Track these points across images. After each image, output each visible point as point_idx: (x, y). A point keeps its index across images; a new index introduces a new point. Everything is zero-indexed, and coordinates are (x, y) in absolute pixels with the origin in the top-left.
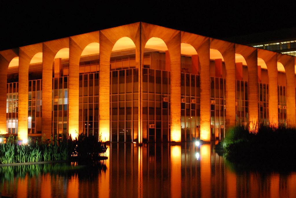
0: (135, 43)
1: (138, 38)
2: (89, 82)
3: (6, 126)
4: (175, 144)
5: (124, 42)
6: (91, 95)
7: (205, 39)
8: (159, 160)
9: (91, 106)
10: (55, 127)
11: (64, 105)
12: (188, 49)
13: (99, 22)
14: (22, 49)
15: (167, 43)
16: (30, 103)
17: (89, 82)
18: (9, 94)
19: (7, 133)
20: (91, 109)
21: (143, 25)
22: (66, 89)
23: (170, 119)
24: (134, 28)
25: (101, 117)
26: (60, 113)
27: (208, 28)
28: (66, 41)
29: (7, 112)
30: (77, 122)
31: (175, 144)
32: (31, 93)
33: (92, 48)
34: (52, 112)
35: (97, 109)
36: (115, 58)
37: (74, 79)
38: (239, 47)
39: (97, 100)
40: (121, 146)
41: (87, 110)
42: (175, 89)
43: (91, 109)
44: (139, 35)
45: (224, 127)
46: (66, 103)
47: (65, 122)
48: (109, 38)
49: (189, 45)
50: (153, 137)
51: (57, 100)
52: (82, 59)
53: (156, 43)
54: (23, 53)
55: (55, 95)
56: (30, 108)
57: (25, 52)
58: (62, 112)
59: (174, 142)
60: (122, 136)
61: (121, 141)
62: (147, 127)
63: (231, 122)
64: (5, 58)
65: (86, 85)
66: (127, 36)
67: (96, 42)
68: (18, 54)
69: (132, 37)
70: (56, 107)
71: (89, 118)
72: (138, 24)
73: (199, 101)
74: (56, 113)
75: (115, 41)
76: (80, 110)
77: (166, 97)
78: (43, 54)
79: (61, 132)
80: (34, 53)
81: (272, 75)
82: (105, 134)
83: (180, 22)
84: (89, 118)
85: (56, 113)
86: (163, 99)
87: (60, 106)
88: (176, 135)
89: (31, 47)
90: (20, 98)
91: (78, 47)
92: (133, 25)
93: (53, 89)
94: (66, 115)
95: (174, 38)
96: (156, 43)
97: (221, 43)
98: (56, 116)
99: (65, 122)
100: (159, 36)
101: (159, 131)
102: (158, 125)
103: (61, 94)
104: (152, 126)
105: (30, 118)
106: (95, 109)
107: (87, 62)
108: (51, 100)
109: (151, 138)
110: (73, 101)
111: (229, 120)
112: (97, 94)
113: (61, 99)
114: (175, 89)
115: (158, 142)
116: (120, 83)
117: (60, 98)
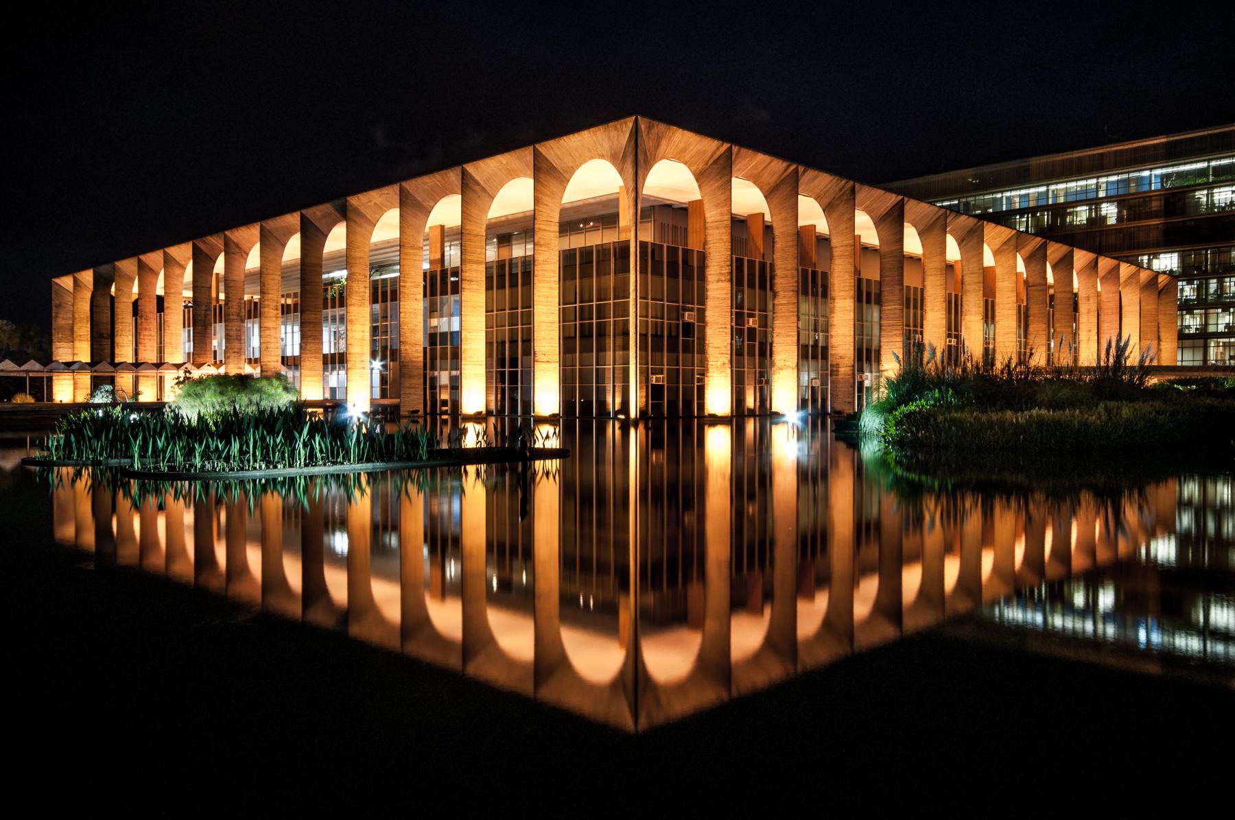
0: (621, 172)
1: (630, 160)
2: (511, 282)
3: (325, 380)
4: (715, 420)
5: (514, 195)
6: (513, 322)
7: (788, 167)
8: (673, 459)
9: (513, 333)
10: (433, 387)
11: (452, 333)
12: (747, 197)
13: (529, 120)
14: (354, 201)
15: (700, 176)
16: (374, 330)
17: (511, 282)
18: (330, 312)
19: (57, 281)
20: (513, 342)
21: (643, 123)
22: (456, 297)
23: (703, 363)
24: (618, 134)
25: (539, 357)
26: (444, 351)
27: (801, 141)
28: (453, 176)
29: (326, 350)
30: (482, 370)
31: (715, 420)
32: (377, 307)
33: (514, 195)
34: (425, 349)
35: (528, 341)
36: (570, 223)
37: (475, 267)
38: (865, 193)
39: (528, 319)
40: (586, 430)
41: (504, 343)
42: (718, 291)
43: (513, 342)
44: (631, 149)
45: (817, 383)
46: (456, 328)
47: (454, 373)
48: (556, 163)
49: (750, 183)
50: (661, 405)
51: (434, 322)
52: (563, 211)
53: (671, 179)
54: (357, 211)
55: (432, 311)
56: (373, 342)
57: (362, 209)
58: (444, 348)
59: (713, 416)
60: (586, 406)
61: (583, 415)
62: (647, 381)
63: (842, 370)
64: (317, 224)
65: (501, 286)
66: (602, 157)
67: (526, 176)
68: (344, 213)
69: (614, 159)
70: (434, 338)
71: (510, 366)
72: (629, 123)
73: (764, 322)
74: (433, 352)
75: (572, 171)
76: (489, 344)
77: (692, 310)
78: (401, 215)
79: (445, 396)
80: (381, 210)
81: (932, 265)
82: (547, 395)
83: (733, 122)
84: (510, 366)
85: (433, 352)
86: (683, 315)
87: (444, 335)
88: (718, 398)
89: (375, 196)
90: (351, 316)
91: (483, 189)
92: (617, 124)
93: (425, 296)
94: (456, 357)
95: (715, 162)
96: (593, 175)
97: (824, 180)
98: (433, 358)
99: (454, 373)
100: (678, 157)
101: (674, 391)
102: (673, 376)
103: (445, 308)
104: (657, 379)
105: (377, 364)
106: (523, 341)
107: (504, 233)
108: (421, 319)
109: (657, 407)
110: (472, 323)
111: (838, 365)
112: (529, 303)
113: (445, 319)
114: (718, 291)
115: (676, 419)
116: (581, 278)
117: (442, 316)
